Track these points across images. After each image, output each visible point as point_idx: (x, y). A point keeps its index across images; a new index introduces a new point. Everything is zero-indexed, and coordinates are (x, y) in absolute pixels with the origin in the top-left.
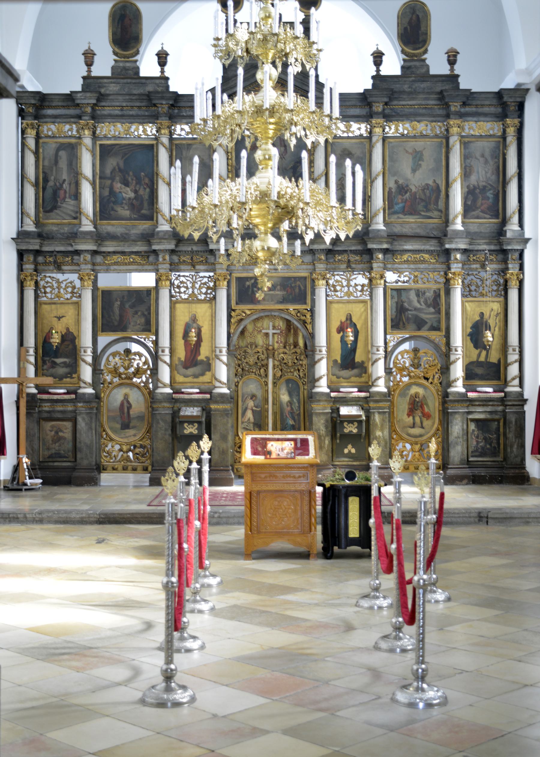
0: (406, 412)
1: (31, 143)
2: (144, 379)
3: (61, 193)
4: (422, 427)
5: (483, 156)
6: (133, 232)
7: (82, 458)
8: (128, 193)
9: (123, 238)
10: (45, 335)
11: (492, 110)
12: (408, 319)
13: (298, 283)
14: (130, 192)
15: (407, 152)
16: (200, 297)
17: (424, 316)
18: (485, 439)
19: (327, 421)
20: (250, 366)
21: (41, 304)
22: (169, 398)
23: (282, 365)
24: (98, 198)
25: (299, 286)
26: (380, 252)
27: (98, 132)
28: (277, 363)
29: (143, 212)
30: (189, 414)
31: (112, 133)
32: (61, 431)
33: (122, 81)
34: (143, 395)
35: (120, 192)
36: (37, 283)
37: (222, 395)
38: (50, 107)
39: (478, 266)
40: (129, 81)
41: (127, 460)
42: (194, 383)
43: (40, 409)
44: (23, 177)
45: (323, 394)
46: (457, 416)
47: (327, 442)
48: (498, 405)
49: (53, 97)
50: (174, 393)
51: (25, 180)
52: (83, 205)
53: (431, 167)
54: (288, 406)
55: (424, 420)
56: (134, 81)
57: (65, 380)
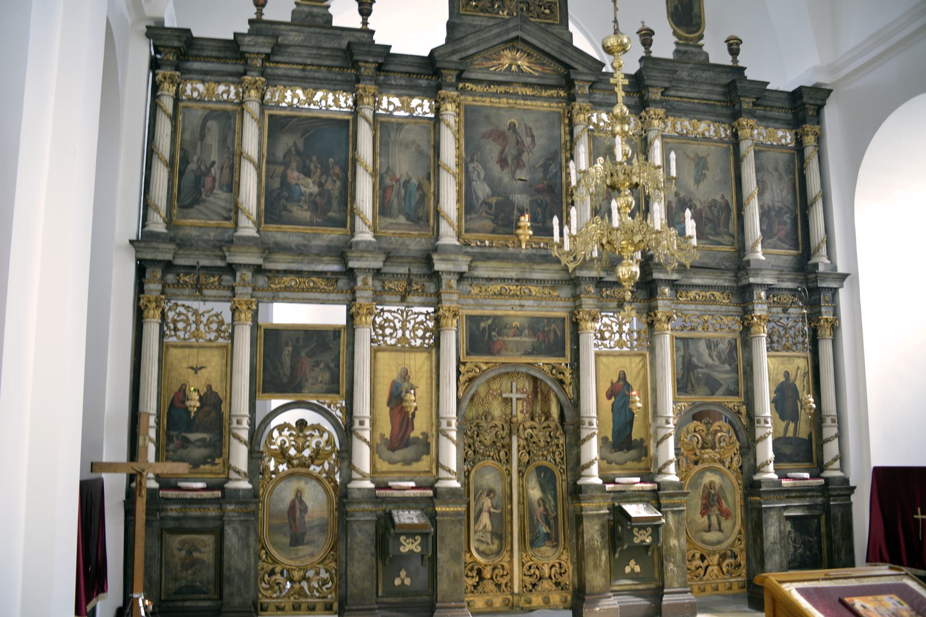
0: (699, 510)
1: (167, 103)
2: (326, 466)
3: (208, 181)
4: (720, 530)
5: (776, 170)
6: (316, 242)
7: (232, 595)
8: (309, 187)
9: (301, 251)
10: (172, 395)
11: (781, 114)
12: (698, 380)
13: (553, 326)
14: (311, 184)
15: (688, 157)
16: (413, 343)
17: (718, 376)
18: (804, 543)
19: (603, 526)
20: (486, 446)
21: (167, 347)
22: (371, 497)
23: (529, 445)
24: (263, 191)
25: (555, 331)
26: (667, 286)
27: (268, 97)
28: (523, 442)
29: (331, 214)
30: (408, 521)
31: (289, 99)
32: (197, 550)
33: (307, 29)
34: (326, 491)
35: (297, 184)
36: (163, 315)
37: (452, 492)
38: (198, 58)
39: (780, 310)
40: (317, 30)
41: (300, 595)
42: (404, 472)
43: (163, 514)
44: (151, 152)
45: (595, 487)
46: (772, 513)
47: (604, 558)
48: (817, 496)
49: (205, 43)
50: (377, 488)
51: (155, 157)
52: (242, 198)
53: (717, 179)
54: (540, 506)
55: (723, 519)
56: (324, 31)
57: (202, 467)
